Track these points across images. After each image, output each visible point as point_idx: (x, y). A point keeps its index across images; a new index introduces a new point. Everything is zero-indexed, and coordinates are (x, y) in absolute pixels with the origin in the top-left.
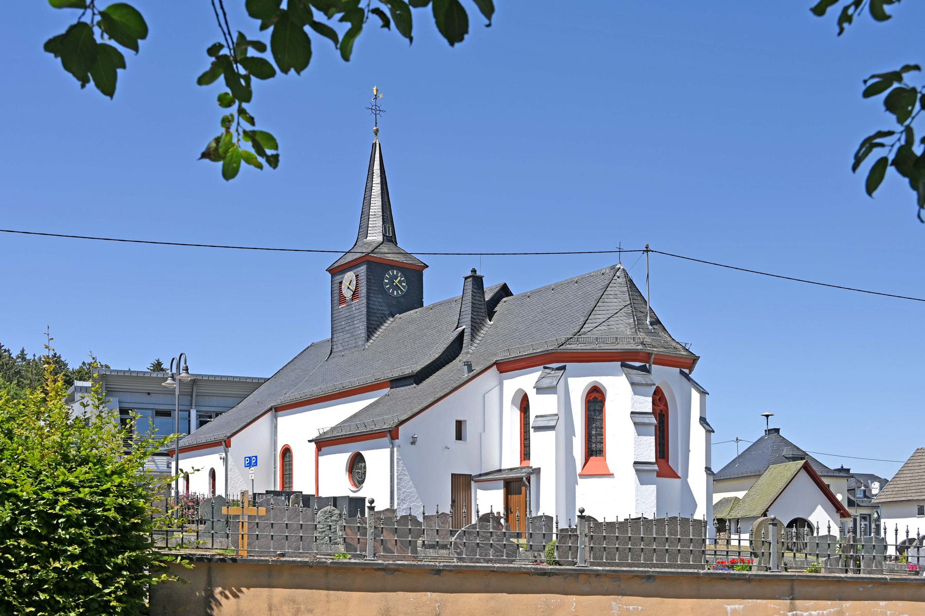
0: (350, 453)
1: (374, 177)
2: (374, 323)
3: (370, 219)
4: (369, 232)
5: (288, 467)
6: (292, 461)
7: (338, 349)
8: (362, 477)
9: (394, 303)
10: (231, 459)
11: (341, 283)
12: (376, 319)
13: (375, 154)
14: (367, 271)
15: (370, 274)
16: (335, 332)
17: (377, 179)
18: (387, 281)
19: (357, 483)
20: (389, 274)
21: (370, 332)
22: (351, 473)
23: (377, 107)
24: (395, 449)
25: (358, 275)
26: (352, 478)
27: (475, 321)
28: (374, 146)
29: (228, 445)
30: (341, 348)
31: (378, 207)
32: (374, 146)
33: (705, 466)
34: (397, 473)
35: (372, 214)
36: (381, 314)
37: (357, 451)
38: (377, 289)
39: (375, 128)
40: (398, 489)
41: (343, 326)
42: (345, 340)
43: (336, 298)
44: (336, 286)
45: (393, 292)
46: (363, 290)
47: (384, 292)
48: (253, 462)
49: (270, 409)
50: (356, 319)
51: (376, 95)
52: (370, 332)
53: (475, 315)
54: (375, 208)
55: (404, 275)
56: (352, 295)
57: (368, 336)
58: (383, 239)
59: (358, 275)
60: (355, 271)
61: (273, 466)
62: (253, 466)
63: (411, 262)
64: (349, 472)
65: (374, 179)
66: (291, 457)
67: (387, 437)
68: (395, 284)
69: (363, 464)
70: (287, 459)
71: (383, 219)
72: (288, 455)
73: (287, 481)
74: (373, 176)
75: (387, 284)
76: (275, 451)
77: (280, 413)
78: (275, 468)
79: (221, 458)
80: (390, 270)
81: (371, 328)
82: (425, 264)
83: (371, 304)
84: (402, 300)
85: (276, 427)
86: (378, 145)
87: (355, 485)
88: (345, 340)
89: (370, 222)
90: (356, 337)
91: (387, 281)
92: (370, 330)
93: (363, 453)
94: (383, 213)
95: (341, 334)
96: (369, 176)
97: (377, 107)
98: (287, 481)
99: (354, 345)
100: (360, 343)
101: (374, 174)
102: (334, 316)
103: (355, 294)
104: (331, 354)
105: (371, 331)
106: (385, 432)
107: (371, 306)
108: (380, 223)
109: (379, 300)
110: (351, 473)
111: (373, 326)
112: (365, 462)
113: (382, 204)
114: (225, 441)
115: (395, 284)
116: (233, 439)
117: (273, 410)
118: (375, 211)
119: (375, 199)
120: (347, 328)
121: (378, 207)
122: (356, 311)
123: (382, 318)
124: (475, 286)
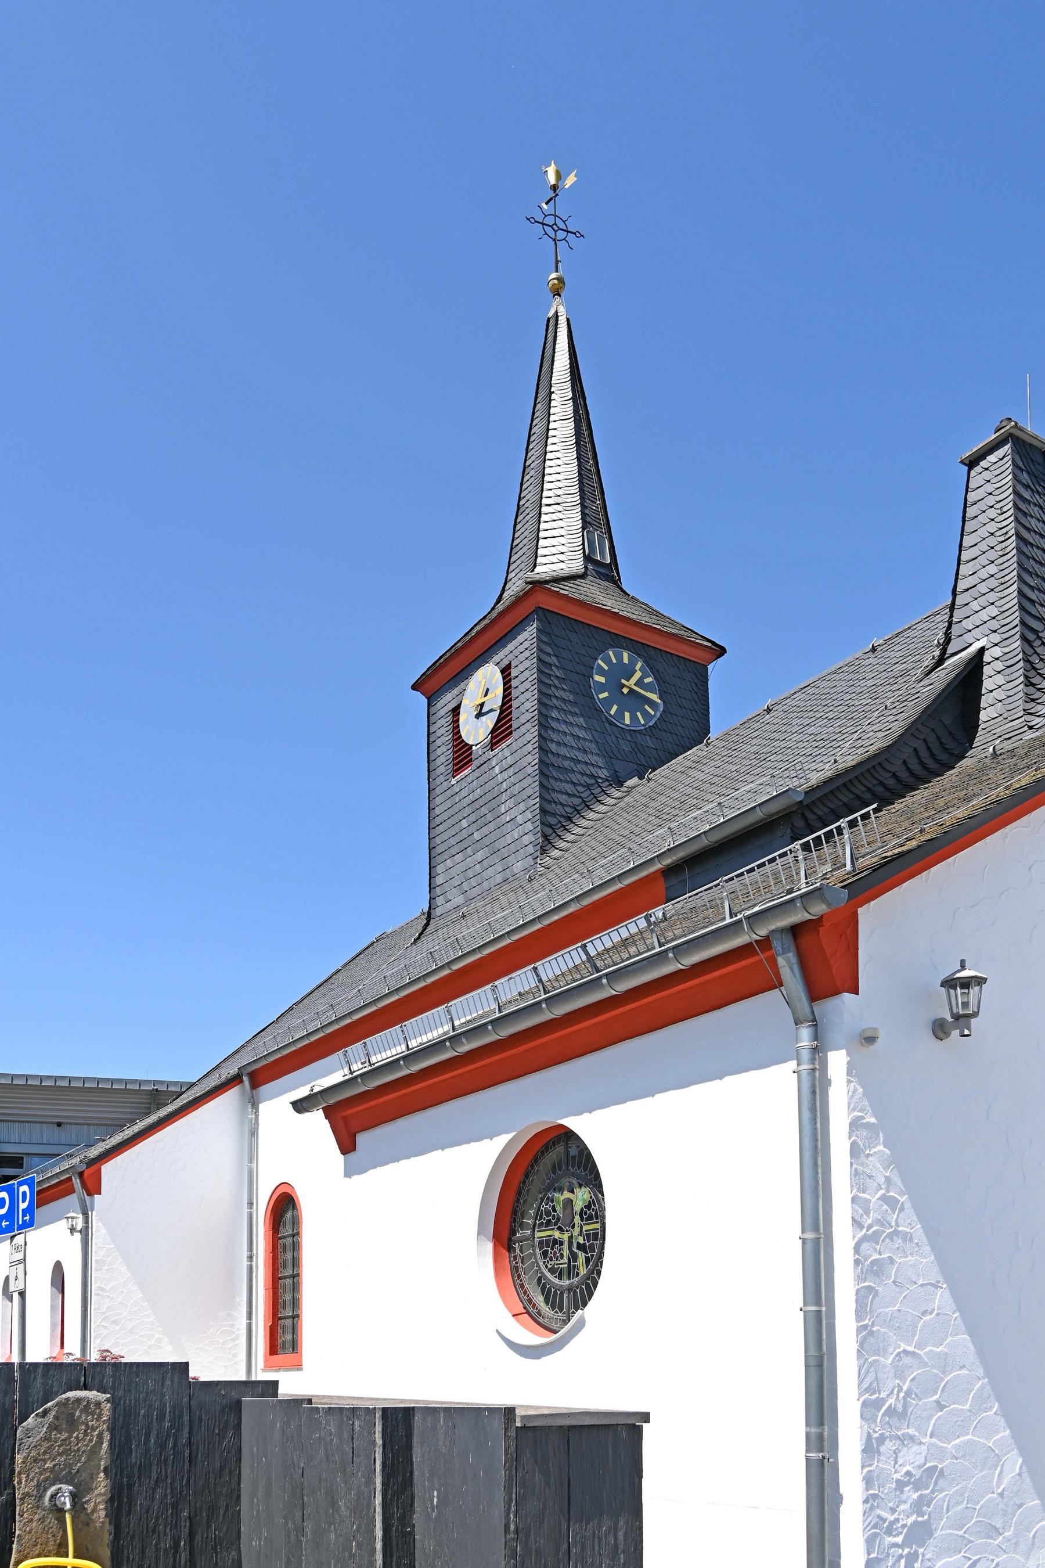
0: (502, 1140)
1: (553, 403)
2: (563, 798)
3: (544, 518)
4: (540, 552)
5: (289, 1256)
6: (298, 1234)
7: (449, 906)
8: (571, 1271)
9: (625, 747)
10: (103, 1231)
11: (456, 711)
12: (570, 789)
13: (555, 344)
14: (539, 640)
15: (549, 650)
16: (438, 859)
17: (561, 406)
18: (602, 680)
19: (540, 1300)
20: (608, 661)
21: (550, 826)
22: (510, 1249)
23: (558, 221)
24: (837, 1061)
25: (509, 666)
26: (515, 1271)
27: (1033, 611)
28: (552, 323)
29: (93, 1187)
30: (460, 900)
31: (567, 483)
32: (552, 323)
33: (511, 1316)
34: (857, 1223)
35: (550, 494)
36: (583, 774)
37: (540, 1119)
38: (571, 698)
39: (554, 275)
40: (866, 1336)
41: (464, 834)
42: (470, 873)
43: (444, 753)
44: (443, 724)
45: (620, 714)
46: (526, 704)
47: (593, 712)
48: (23, 1206)
49: (235, 1080)
50: (504, 797)
51: (554, 188)
52: (550, 826)
53: (1032, 588)
54: (559, 484)
55: (651, 667)
56: (492, 732)
57: (545, 837)
58: (586, 568)
59: (509, 666)
60: (497, 658)
61: (245, 1253)
62: (20, 1228)
63: (674, 631)
64: (497, 1238)
65: (552, 411)
66: (296, 1221)
67: (775, 983)
68: (625, 691)
69: (581, 1197)
70: (286, 1231)
71: (583, 514)
72: (289, 1215)
73: (288, 1297)
74: (550, 400)
75: (602, 687)
76: (250, 1204)
77: (265, 1089)
78: (250, 1258)
79: (72, 1230)
80: (612, 646)
81: (554, 815)
82: (713, 643)
83: (552, 741)
84: (649, 741)
85: (254, 1133)
86: (562, 320)
87: (529, 1313)
88: (470, 873)
89: (543, 526)
90: (505, 852)
91: (602, 680)
92: (552, 820)
93: (571, 1123)
94: (582, 498)
95: (459, 858)
96: (538, 406)
97: (558, 221)
98: (288, 1297)
99: (499, 878)
100: (518, 867)
101: (553, 396)
102: (437, 811)
103: (500, 732)
104: (427, 925)
105: (546, 844)
106: (765, 943)
107: (553, 747)
108: (574, 519)
109: (576, 731)
110: (510, 1249)
111: (559, 809)
112: (592, 1178)
113: (580, 474)
114: (81, 1175)
115: (625, 691)
116: (107, 1170)
117: (246, 1079)
118: (559, 492)
119: (558, 462)
120: (477, 836)
121: (568, 468)
122: (505, 775)
123: (588, 786)
124: (1025, 477)
